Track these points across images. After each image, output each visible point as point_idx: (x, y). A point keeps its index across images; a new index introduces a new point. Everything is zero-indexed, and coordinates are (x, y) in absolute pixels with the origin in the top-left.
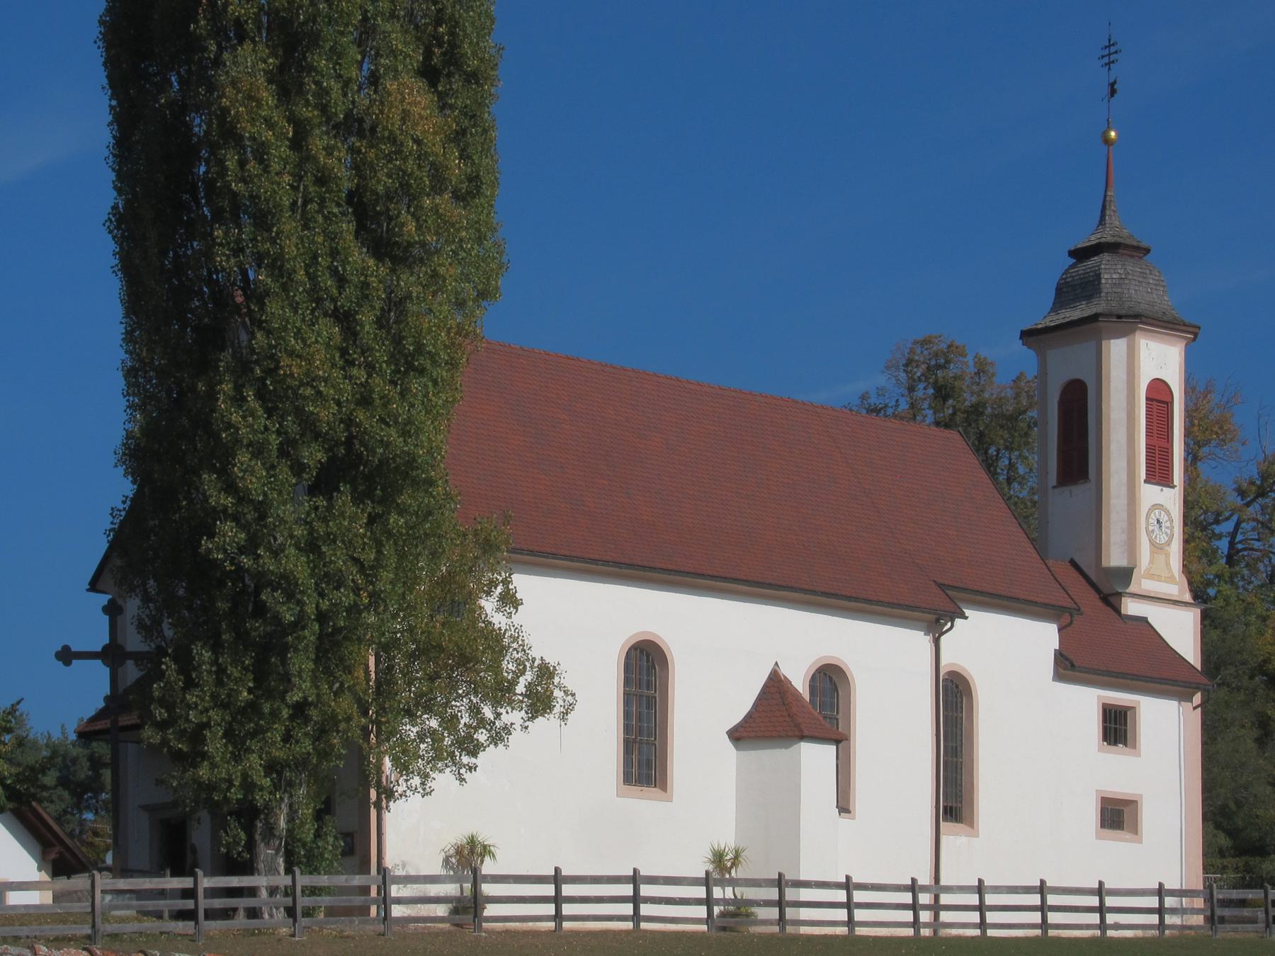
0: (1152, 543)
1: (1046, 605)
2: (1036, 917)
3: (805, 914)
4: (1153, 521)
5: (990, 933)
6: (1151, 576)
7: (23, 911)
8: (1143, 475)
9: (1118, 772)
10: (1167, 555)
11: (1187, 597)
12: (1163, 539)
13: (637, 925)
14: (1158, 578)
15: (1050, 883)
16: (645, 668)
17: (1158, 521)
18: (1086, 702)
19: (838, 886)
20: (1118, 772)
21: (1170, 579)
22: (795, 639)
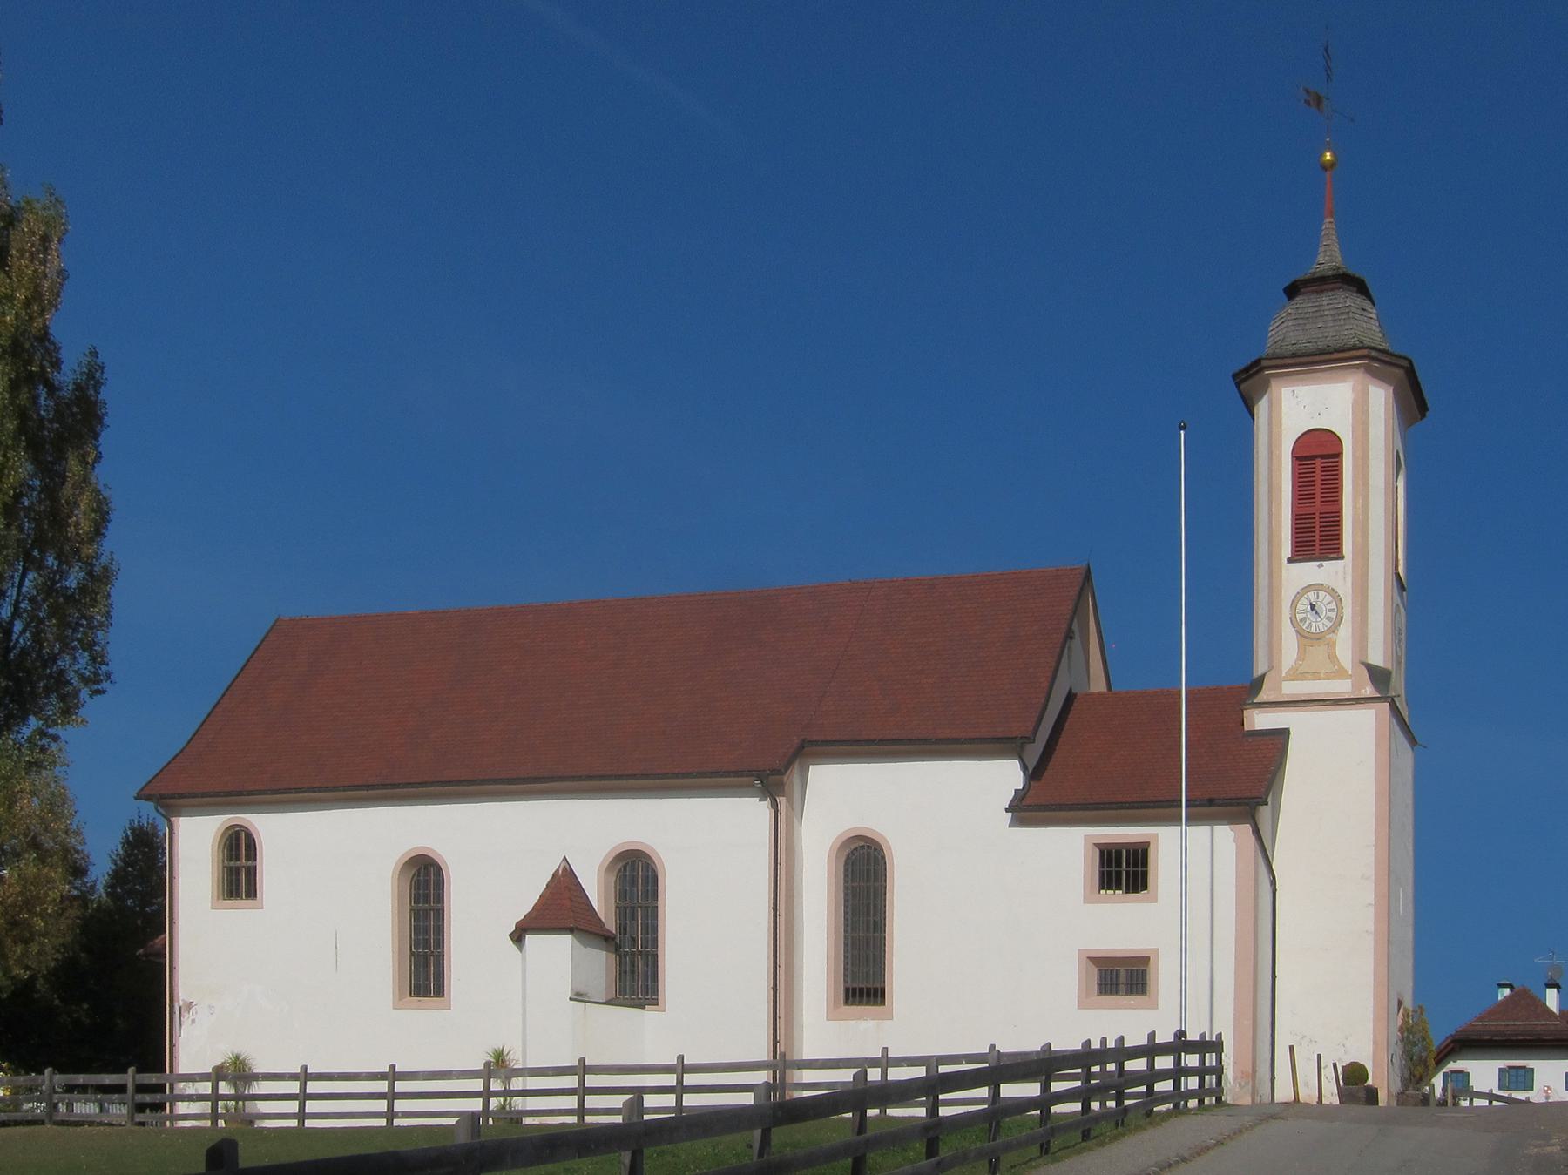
0: (1302, 635)
1: (982, 740)
2: (571, 1102)
3: (264, 1107)
4: (1304, 605)
5: (309, 1123)
6: (1296, 675)
7: (700, 1116)
8: (1286, 550)
9: (1122, 924)
10: (1331, 646)
11: (1369, 691)
12: (1322, 625)
13: (390, 1122)
14: (1316, 676)
15: (516, 1060)
16: (424, 882)
17: (1313, 607)
18: (1069, 848)
19: (293, 1077)
20: (1122, 924)
21: (1340, 674)
22: (582, 832)
